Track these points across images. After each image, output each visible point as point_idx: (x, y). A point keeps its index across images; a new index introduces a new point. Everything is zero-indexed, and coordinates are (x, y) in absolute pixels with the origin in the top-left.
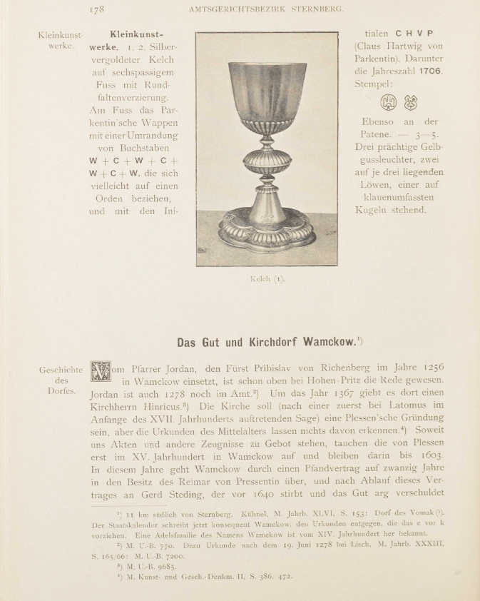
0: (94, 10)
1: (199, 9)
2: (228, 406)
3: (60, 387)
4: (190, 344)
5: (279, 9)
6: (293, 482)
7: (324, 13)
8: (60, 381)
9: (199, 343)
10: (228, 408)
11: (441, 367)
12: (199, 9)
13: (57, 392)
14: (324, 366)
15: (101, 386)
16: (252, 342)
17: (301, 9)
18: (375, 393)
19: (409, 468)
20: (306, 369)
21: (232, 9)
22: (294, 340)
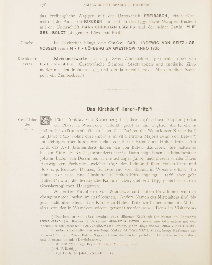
0: (42, 5)
1: (88, 5)
2: (176, 131)
3: (27, 127)
4: (93, 110)
5: (123, 5)
6: (155, 164)
7: (143, 7)
8: (27, 125)
9: (97, 109)
10: (176, 131)
11: (147, 120)
12: (88, 5)
13: (26, 129)
14: (97, 119)
15: (45, 127)
16: (99, 109)
17: (133, 5)
18: (131, 126)
19: (124, 159)
20: (89, 120)
21: (103, 5)
22: (118, 108)
